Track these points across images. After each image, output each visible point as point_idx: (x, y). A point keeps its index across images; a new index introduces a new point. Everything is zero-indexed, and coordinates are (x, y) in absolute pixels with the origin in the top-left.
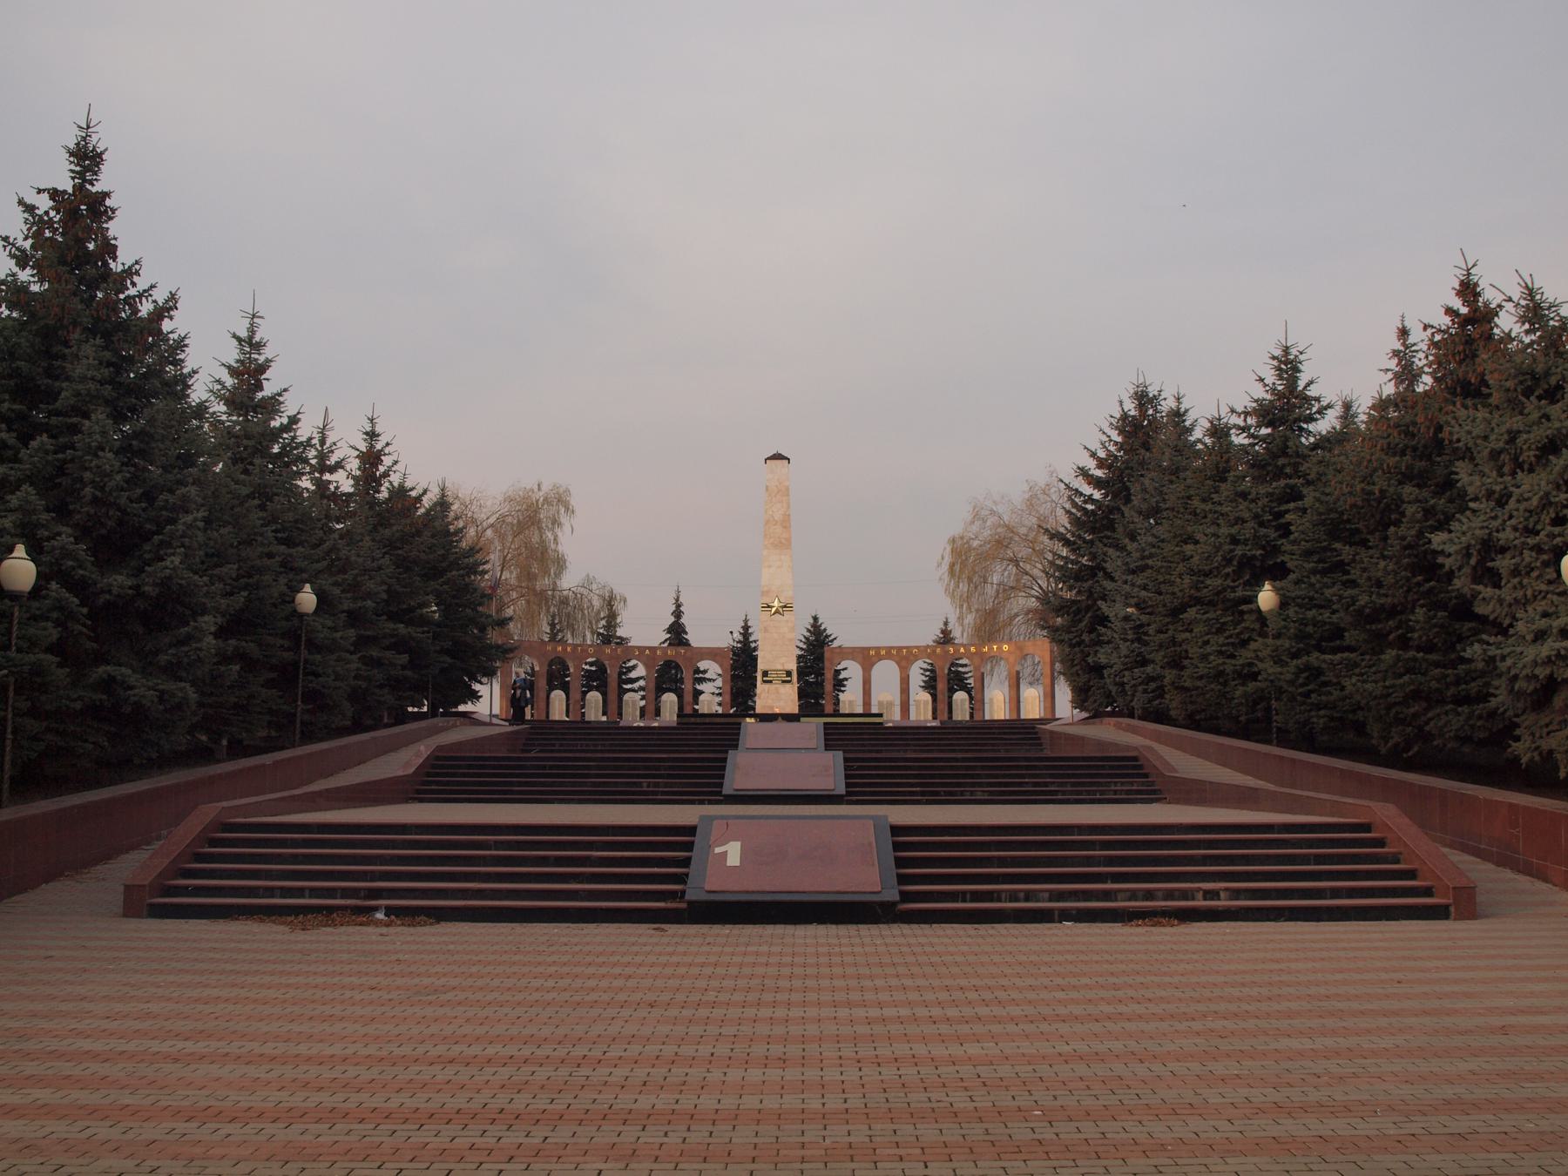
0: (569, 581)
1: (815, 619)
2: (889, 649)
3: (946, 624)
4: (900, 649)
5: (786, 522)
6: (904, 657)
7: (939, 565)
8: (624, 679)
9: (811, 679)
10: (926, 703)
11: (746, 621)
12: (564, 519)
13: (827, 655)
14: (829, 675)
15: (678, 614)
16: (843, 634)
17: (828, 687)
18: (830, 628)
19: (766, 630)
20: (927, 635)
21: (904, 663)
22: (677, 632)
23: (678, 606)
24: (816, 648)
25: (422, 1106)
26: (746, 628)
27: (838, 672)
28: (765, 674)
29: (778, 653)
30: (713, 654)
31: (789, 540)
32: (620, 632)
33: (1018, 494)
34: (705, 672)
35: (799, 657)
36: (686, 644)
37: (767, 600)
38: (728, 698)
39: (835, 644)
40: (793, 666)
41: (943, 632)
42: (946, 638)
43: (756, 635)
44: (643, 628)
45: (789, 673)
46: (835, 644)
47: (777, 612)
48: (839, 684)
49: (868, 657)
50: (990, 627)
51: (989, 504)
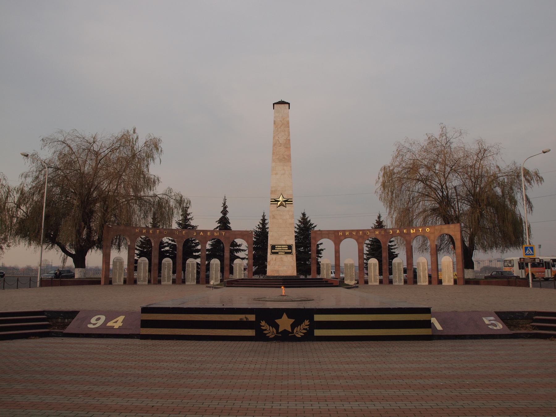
0: (159, 190)
1: (304, 215)
2: (351, 231)
3: (379, 217)
4: (358, 231)
5: (287, 144)
6: (358, 235)
7: (377, 182)
8: (235, 248)
9: (302, 249)
10: (375, 265)
11: (264, 216)
12: (156, 156)
13: (312, 235)
14: (313, 248)
15: (225, 212)
16: (320, 223)
17: (314, 255)
18: (313, 219)
19: (274, 217)
20: (369, 224)
21: (361, 240)
22: (224, 222)
23: (225, 207)
24: (305, 232)
25: (155, 405)
26: (264, 220)
27: (318, 246)
28: (273, 247)
29: (282, 234)
30: (243, 235)
31: (289, 156)
32: (193, 223)
33: (423, 141)
34: (240, 245)
35: (296, 236)
36: (229, 229)
37: (275, 197)
38: (252, 261)
39: (316, 229)
40: (292, 242)
41: (377, 222)
42: (380, 225)
43: (269, 226)
44: (205, 220)
45: (290, 247)
46: (316, 229)
47: (281, 205)
48: (319, 252)
49: (337, 237)
50: (405, 219)
51: (407, 145)
